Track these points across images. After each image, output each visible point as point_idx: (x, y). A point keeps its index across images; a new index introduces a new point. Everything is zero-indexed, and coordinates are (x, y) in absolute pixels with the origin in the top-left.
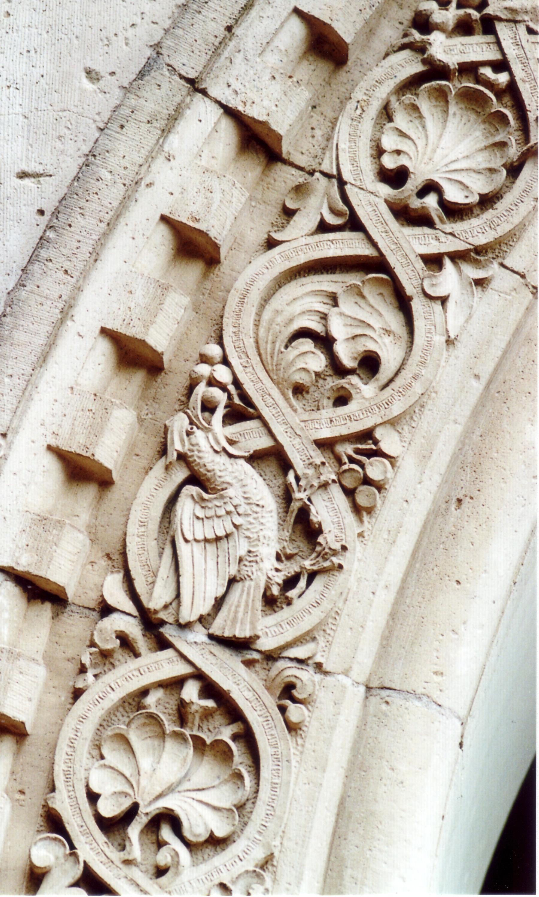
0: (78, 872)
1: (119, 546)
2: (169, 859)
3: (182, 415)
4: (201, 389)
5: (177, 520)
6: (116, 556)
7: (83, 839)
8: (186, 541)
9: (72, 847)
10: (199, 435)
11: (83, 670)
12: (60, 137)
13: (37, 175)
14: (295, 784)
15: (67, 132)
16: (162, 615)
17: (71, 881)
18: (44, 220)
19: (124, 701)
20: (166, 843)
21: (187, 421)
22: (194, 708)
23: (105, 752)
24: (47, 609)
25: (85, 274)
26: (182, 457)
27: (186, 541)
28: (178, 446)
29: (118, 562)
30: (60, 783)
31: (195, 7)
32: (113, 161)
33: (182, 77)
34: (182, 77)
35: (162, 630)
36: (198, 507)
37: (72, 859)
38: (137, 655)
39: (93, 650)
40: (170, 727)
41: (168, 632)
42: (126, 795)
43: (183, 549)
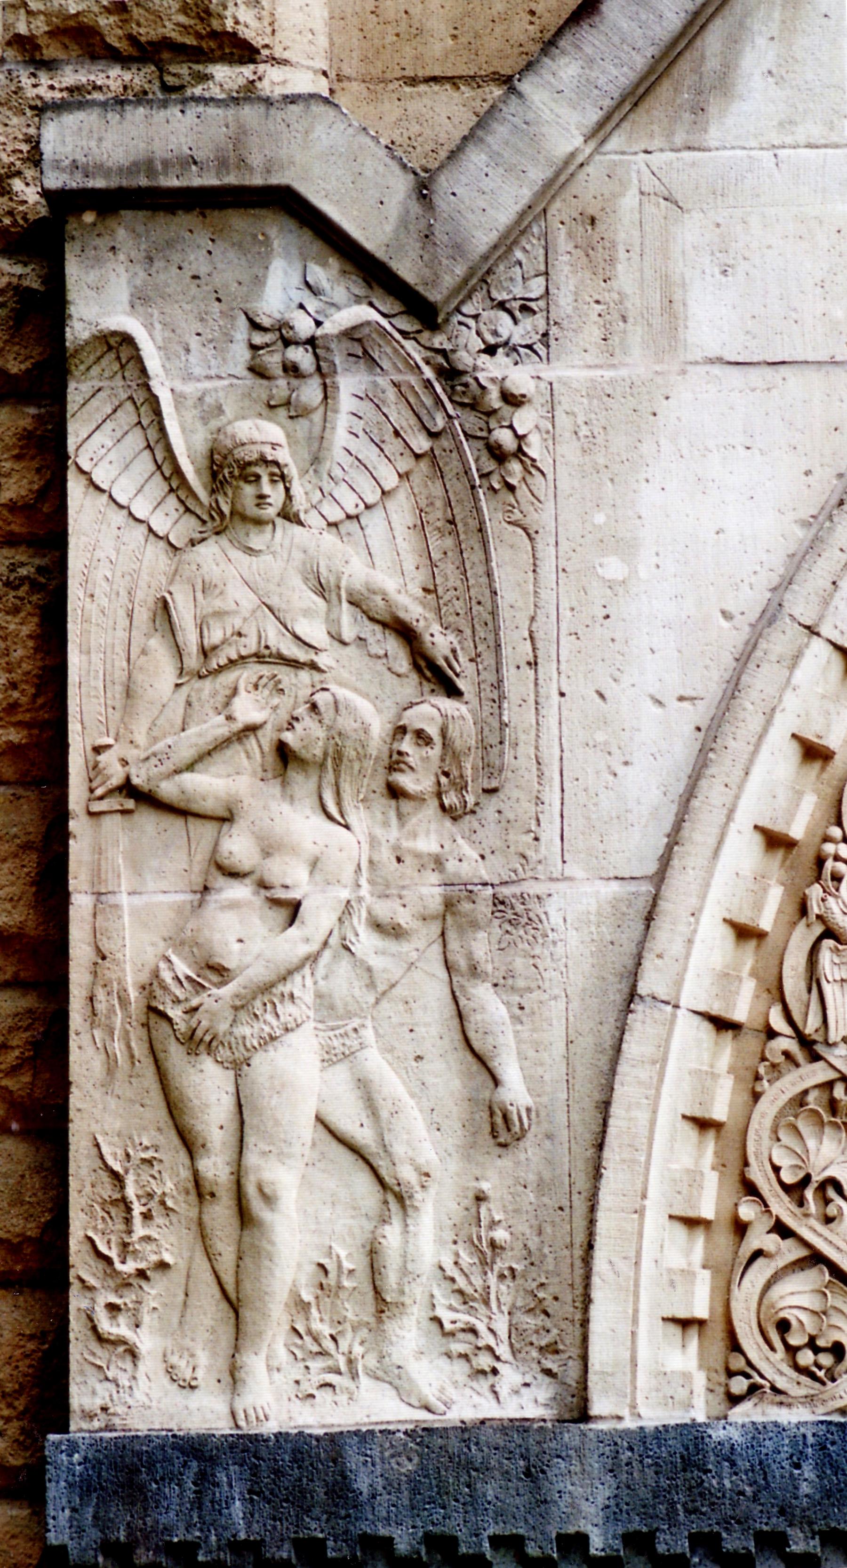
0: (772, 1222)
1: (775, 983)
2: (835, 1212)
3: (817, 885)
4: (829, 864)
5: (820, 966)
6: (775, 991)
7: (773, 1199)
8: (828, 982)
9: (766, 1205)
10: (831, 900)
11: (758, 1078)
12: (706, 667)
13: (692, 699)
14: (428, 384)
15: (712, 663)
16: (815, 1037)
17: (768, 1229)
18: (701, 735)
19: (792, 1100)
20: (832, 1200)
21: (821, 890)
22: (843, 1103)
23: (781, 1136)
24: (730, 1034)
25: (741, 787)
26: (819, 917)
27: (828, 982)
28: (816, 910)
29: (777, 996)
30: (752, 1159)
31: (806, 566)
32: (754, 694)
33: (800, 624)
34: (800, 624)
35: (815, 1047)
36: (835, 956)
37: (767, 1215)
38: (797, 1065)
39: (767, 1063)
40: (826, 1117)
41: (820, 1049)
42: (800, 1168)
43: (827, 989)
